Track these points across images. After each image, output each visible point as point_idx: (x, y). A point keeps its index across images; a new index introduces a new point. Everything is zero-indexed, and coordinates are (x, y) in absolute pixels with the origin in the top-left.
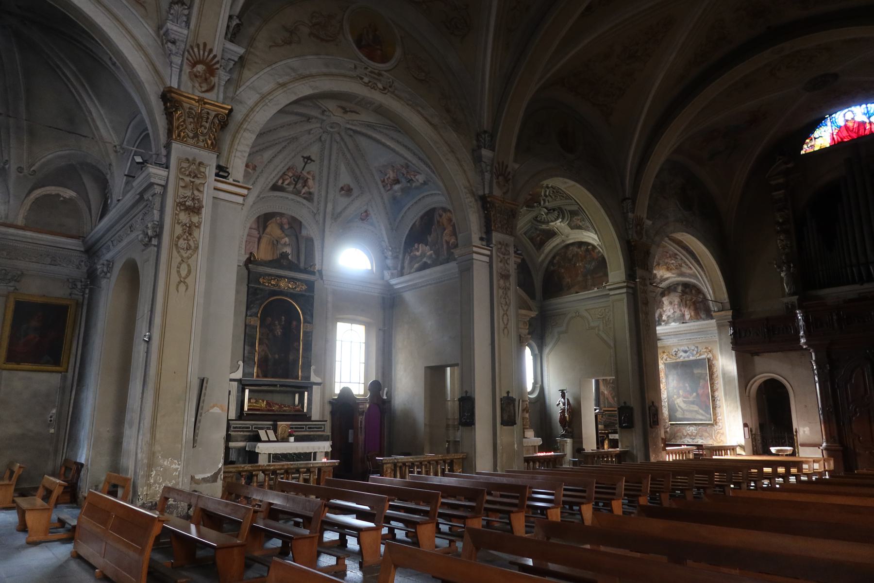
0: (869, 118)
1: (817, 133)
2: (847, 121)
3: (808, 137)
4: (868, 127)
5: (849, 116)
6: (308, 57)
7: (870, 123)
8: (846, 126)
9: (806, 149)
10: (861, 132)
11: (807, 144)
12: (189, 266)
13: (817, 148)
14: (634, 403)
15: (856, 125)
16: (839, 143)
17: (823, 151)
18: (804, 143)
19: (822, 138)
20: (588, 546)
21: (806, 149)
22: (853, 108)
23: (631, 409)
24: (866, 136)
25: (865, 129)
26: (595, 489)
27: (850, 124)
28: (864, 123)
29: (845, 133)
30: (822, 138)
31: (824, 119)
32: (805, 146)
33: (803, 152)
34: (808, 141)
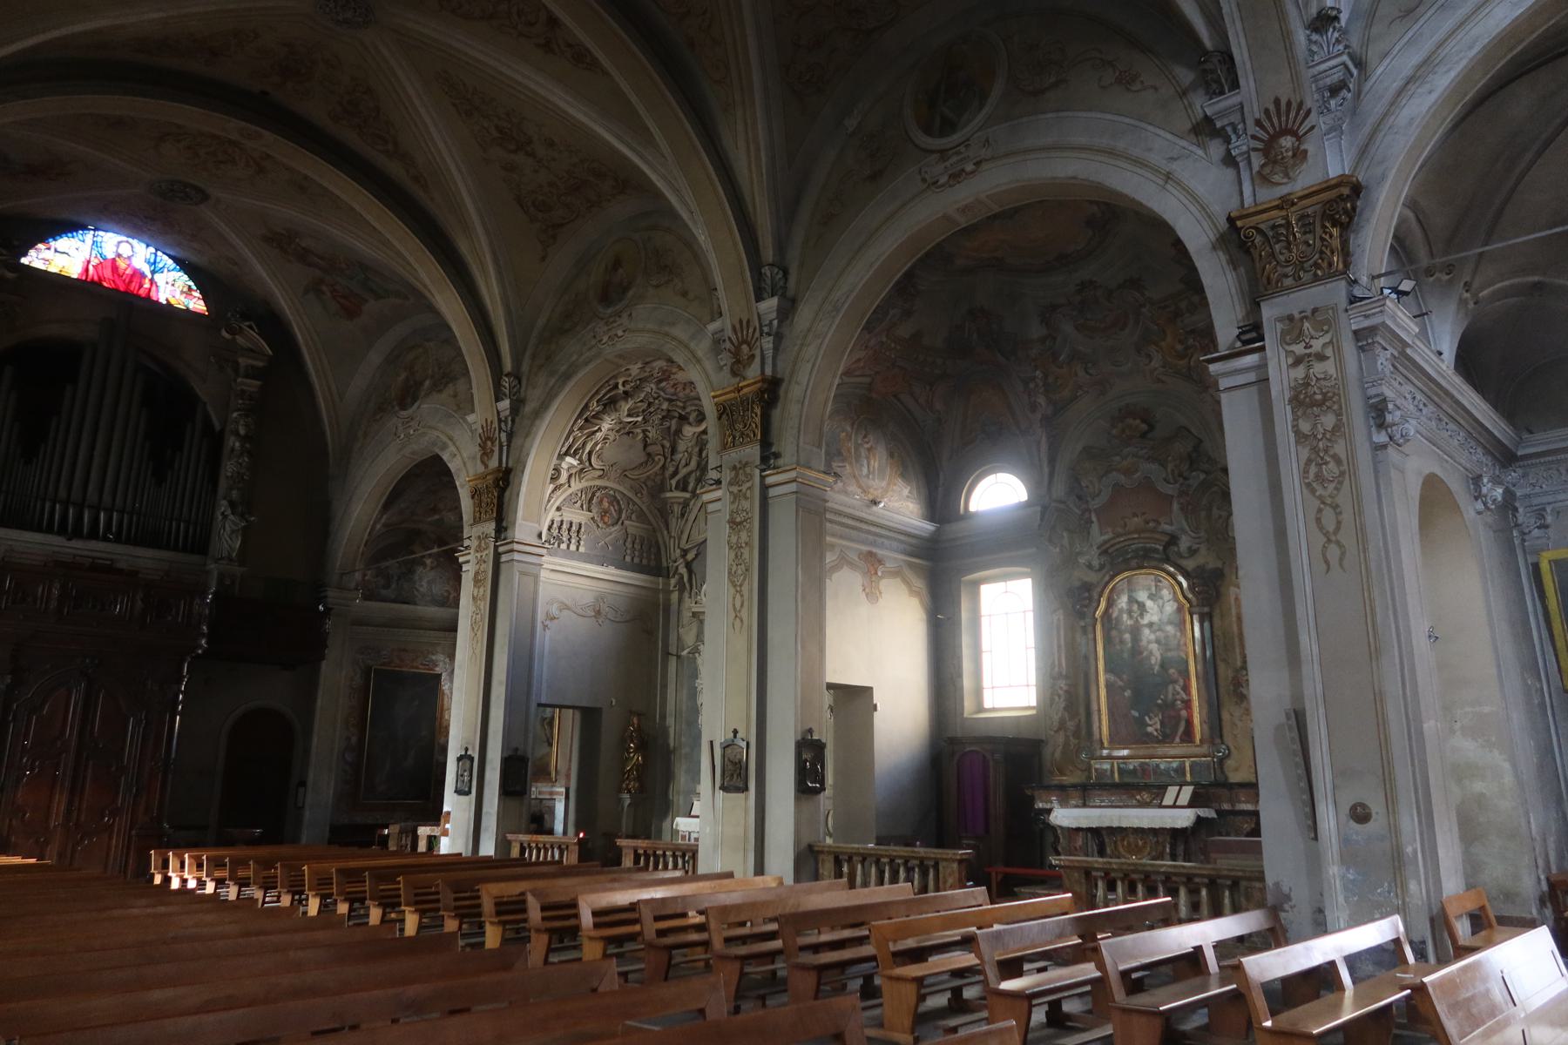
0: (153, 272)
1: (63, 243)
2: (119, 256)
3: (43, 240)
4: (147, 285)
5: (125, 250)
6: (1050, 115)
7: (152, 281)
8: (114, 260)
9: (197, 304)
10: (134, 287)
11: (38, 250)
12: (1321, 528)
13: (53, 269)
14: (825, 732)
15: (129, 272)
16: (92, 281)
17: (58, 282)
18: (32, 246)
19: (65, 256)
20: (1125, 752)
21: (197, 304)
22: (135, 242)
23: (818, 748)
24: (138, 296)
25: (141, 286)
26: (886, 886)
27: (122, 264)
28: (143, 276)
29: (108, 273)
30: (65, 256)
31: (84, 228)
32: (32, 252)
33: (24, 261)
34: (40, 246)
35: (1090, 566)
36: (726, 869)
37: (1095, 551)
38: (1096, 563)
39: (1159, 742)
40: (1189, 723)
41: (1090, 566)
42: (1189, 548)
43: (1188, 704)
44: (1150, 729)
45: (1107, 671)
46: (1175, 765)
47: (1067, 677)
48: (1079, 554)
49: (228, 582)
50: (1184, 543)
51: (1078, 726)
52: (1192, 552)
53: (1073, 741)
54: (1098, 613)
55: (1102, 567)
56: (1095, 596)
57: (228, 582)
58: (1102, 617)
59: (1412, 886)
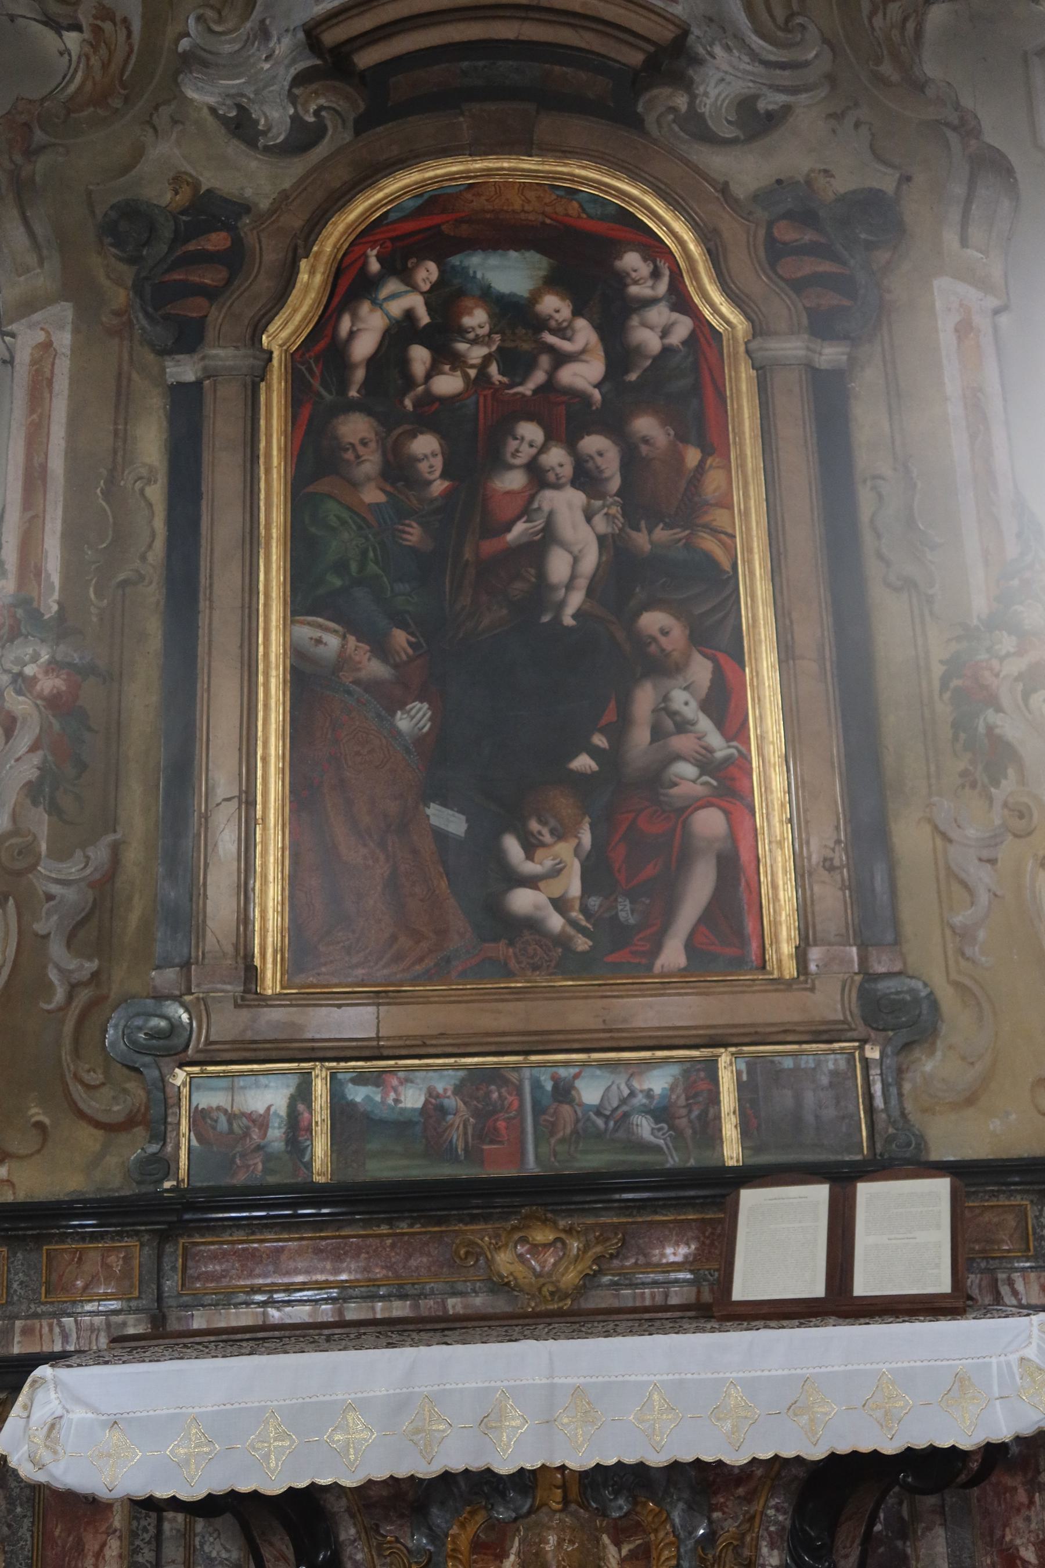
35: (241, 126)
36: (840, 984)
37: (282, 55)
38: (275, 116)
39: (578, 965)
40: (735, 872)
41: (241, 126)
42: (746, 105)
43: (730, 783)
44: (523, 901)
45: (306, 598)
46: (658, 1082)
47: (62, 628)
48: (189, 61)
49: (549, 880)
50: (722, 81)
51: (105, 887)
52: (757, 123)
53: (63, 963)
54: (282, 334)
55: (303, 138)
56: (270, 253)
57: (549, 880)
58: (298, 362)
59: (230, 352)
